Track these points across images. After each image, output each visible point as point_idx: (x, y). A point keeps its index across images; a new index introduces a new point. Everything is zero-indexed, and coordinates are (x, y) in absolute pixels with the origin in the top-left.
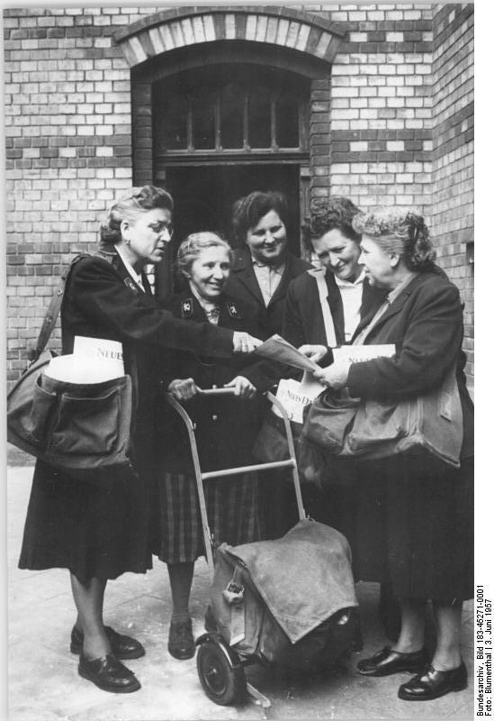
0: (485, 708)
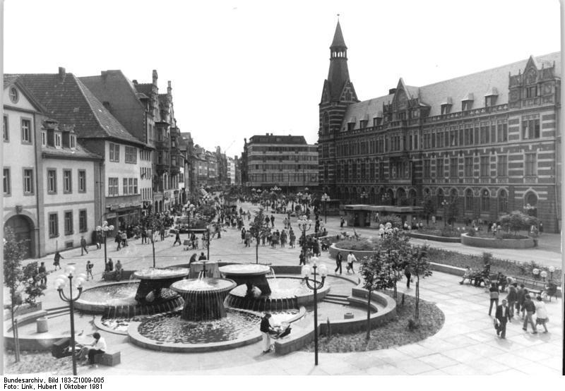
0: (10, 384)
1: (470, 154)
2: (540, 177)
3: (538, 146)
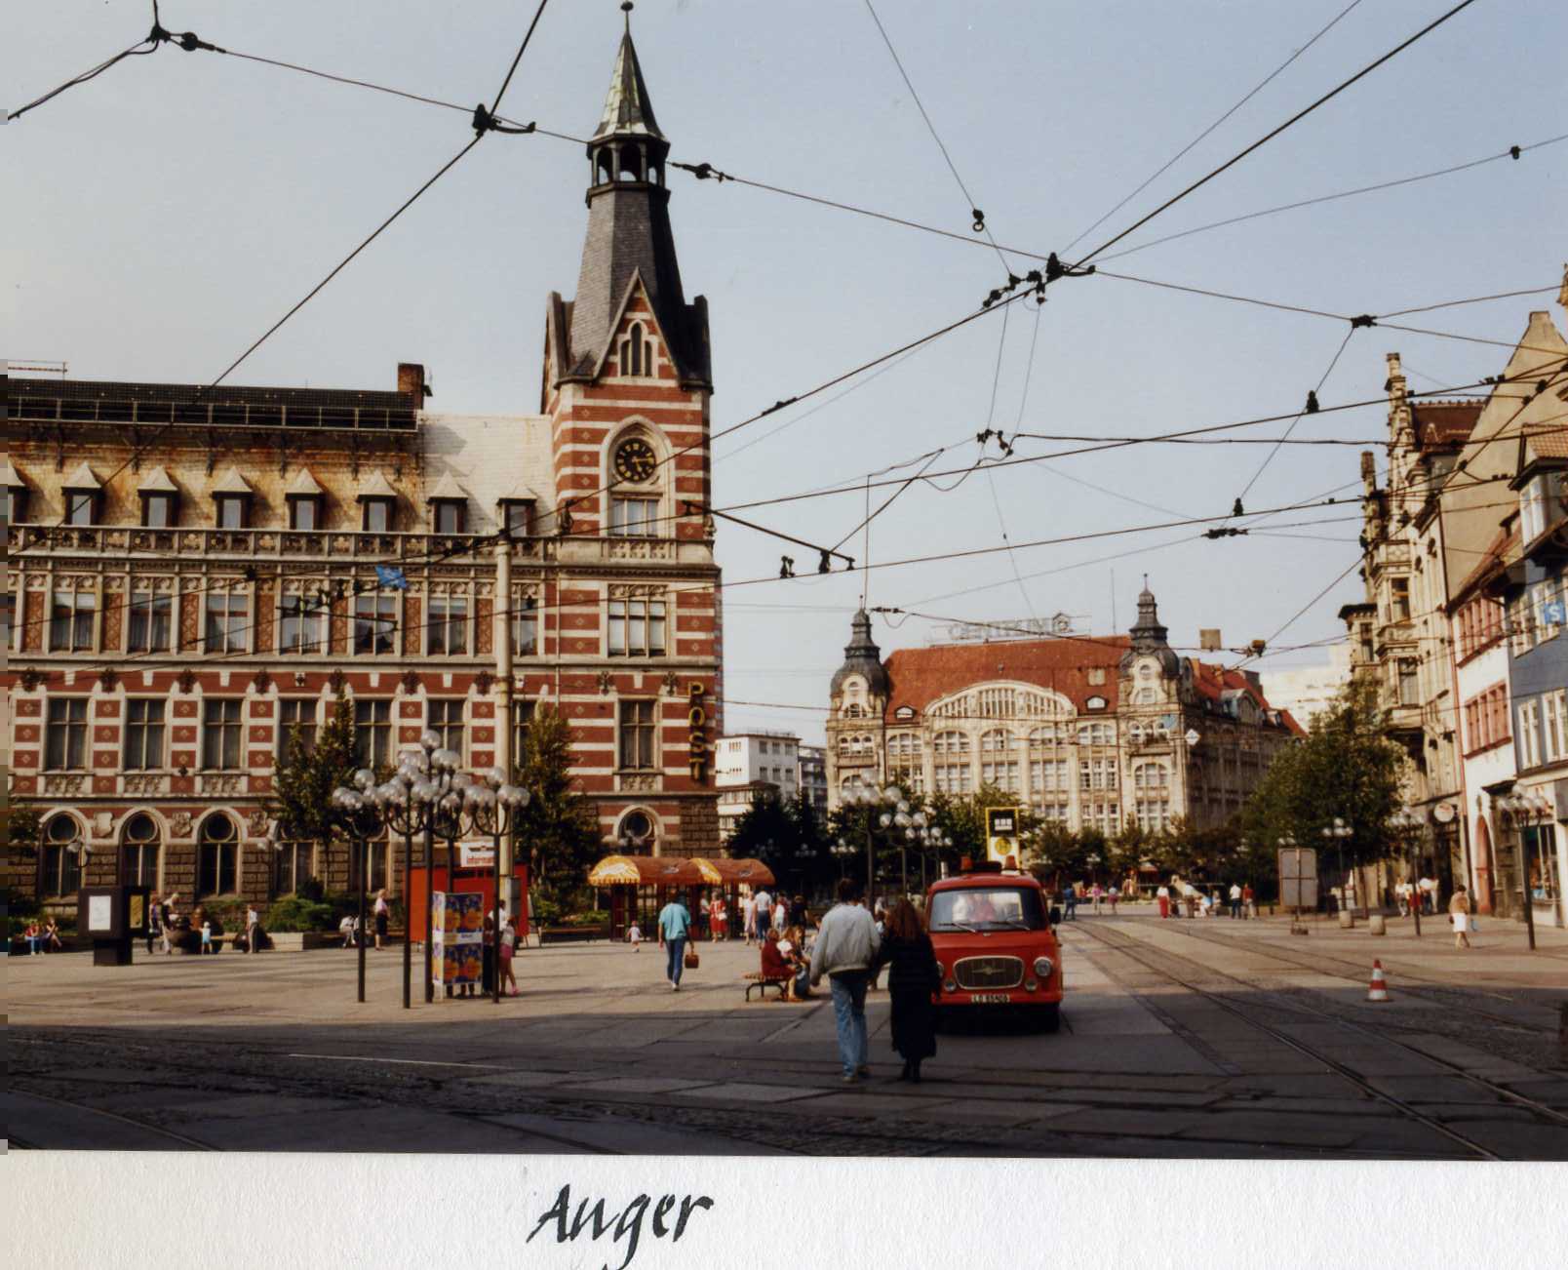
1: (154, 688)
2: (671, 771)
3: (664, 680)
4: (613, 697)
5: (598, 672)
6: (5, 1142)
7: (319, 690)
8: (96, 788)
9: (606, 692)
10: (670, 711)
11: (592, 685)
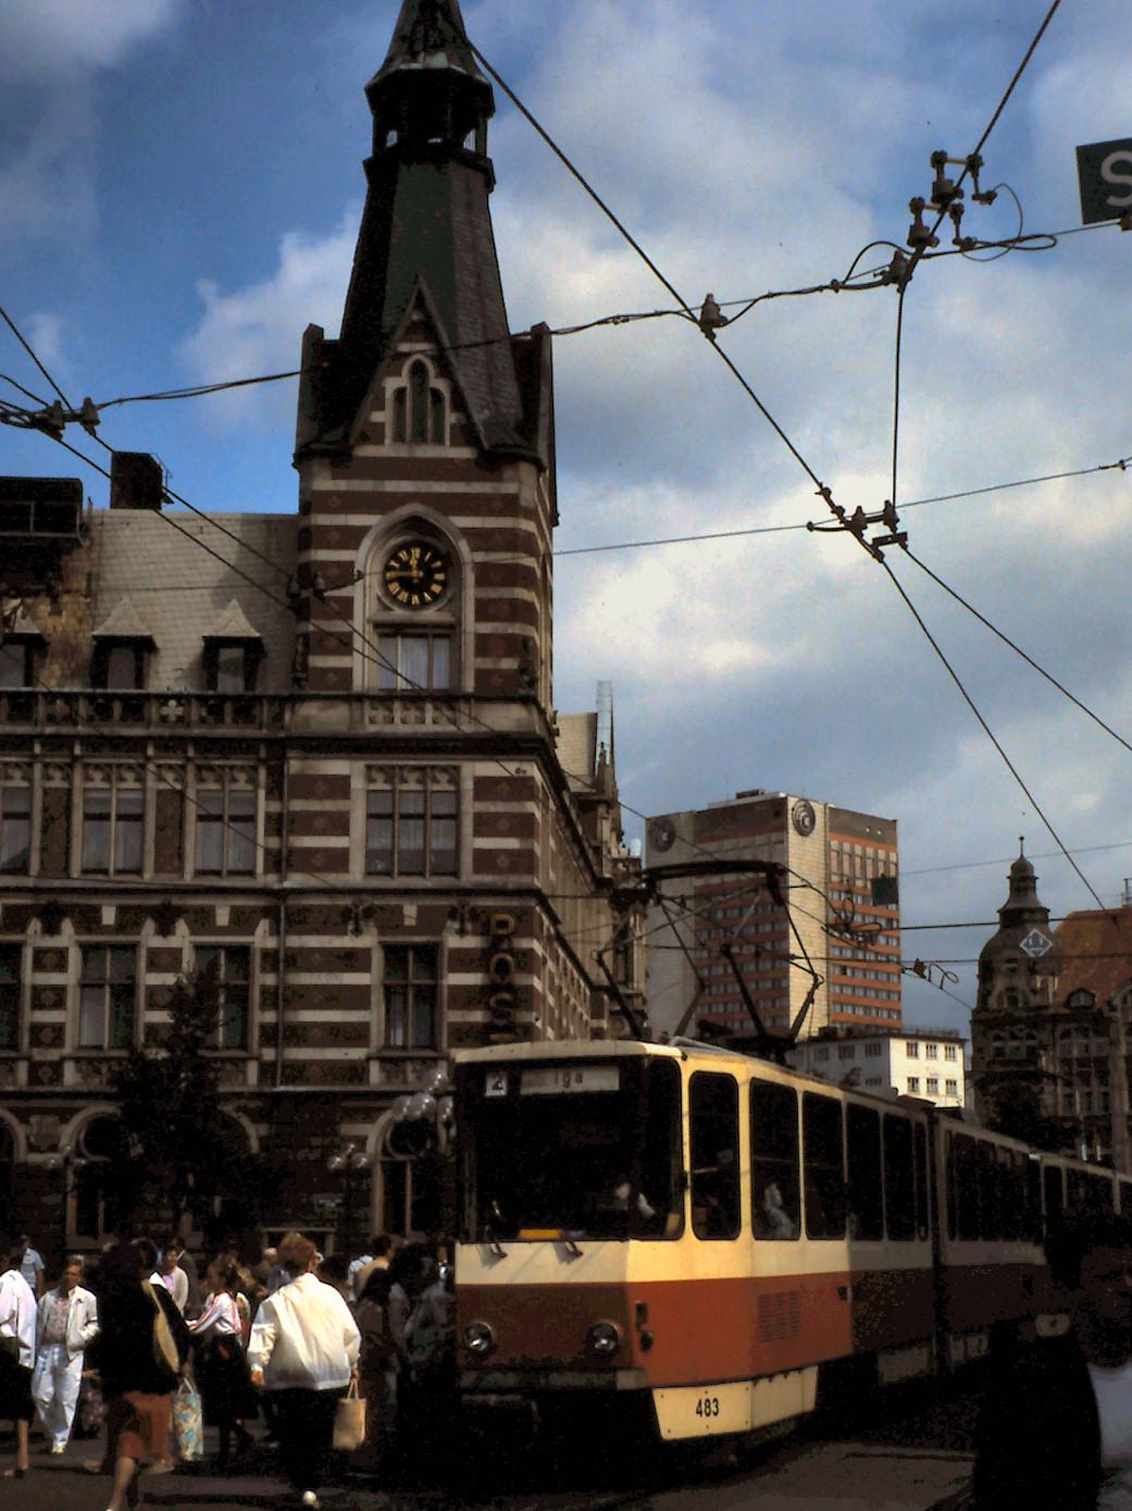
3: (453, 914)
4: (368, 940)
5: (346, 901)
6: (1099, 1508)
7: (23, 930)
8: (33, 1078)
9: (357, 932)
10: (462, 961)
11: (347, 919)
